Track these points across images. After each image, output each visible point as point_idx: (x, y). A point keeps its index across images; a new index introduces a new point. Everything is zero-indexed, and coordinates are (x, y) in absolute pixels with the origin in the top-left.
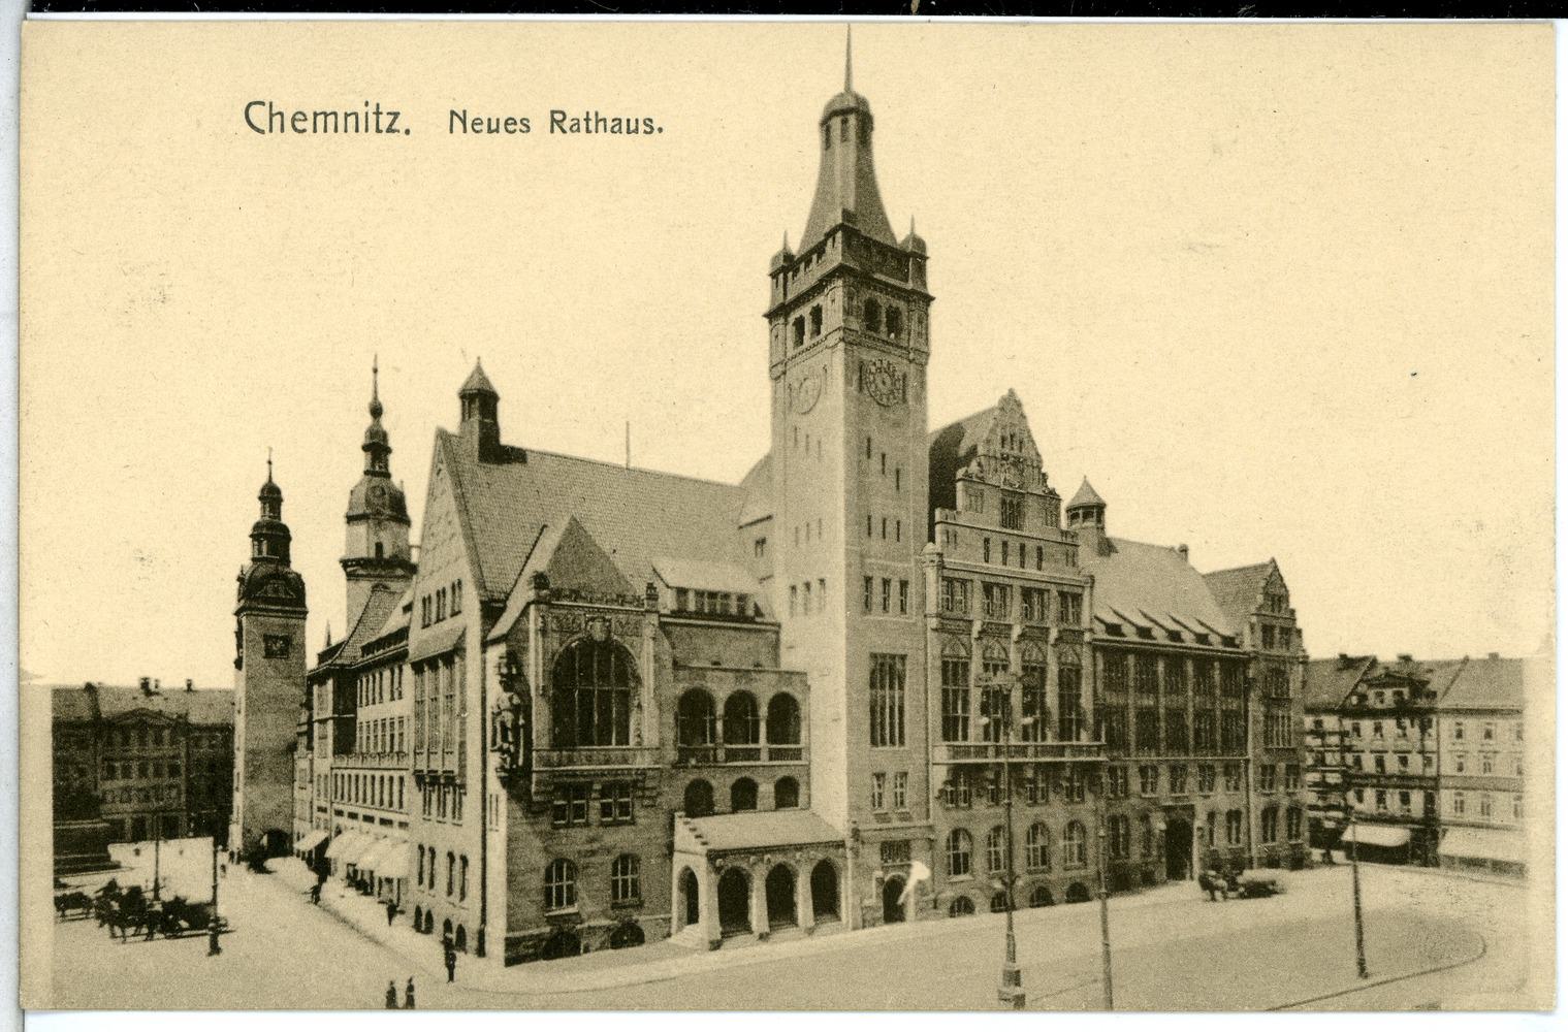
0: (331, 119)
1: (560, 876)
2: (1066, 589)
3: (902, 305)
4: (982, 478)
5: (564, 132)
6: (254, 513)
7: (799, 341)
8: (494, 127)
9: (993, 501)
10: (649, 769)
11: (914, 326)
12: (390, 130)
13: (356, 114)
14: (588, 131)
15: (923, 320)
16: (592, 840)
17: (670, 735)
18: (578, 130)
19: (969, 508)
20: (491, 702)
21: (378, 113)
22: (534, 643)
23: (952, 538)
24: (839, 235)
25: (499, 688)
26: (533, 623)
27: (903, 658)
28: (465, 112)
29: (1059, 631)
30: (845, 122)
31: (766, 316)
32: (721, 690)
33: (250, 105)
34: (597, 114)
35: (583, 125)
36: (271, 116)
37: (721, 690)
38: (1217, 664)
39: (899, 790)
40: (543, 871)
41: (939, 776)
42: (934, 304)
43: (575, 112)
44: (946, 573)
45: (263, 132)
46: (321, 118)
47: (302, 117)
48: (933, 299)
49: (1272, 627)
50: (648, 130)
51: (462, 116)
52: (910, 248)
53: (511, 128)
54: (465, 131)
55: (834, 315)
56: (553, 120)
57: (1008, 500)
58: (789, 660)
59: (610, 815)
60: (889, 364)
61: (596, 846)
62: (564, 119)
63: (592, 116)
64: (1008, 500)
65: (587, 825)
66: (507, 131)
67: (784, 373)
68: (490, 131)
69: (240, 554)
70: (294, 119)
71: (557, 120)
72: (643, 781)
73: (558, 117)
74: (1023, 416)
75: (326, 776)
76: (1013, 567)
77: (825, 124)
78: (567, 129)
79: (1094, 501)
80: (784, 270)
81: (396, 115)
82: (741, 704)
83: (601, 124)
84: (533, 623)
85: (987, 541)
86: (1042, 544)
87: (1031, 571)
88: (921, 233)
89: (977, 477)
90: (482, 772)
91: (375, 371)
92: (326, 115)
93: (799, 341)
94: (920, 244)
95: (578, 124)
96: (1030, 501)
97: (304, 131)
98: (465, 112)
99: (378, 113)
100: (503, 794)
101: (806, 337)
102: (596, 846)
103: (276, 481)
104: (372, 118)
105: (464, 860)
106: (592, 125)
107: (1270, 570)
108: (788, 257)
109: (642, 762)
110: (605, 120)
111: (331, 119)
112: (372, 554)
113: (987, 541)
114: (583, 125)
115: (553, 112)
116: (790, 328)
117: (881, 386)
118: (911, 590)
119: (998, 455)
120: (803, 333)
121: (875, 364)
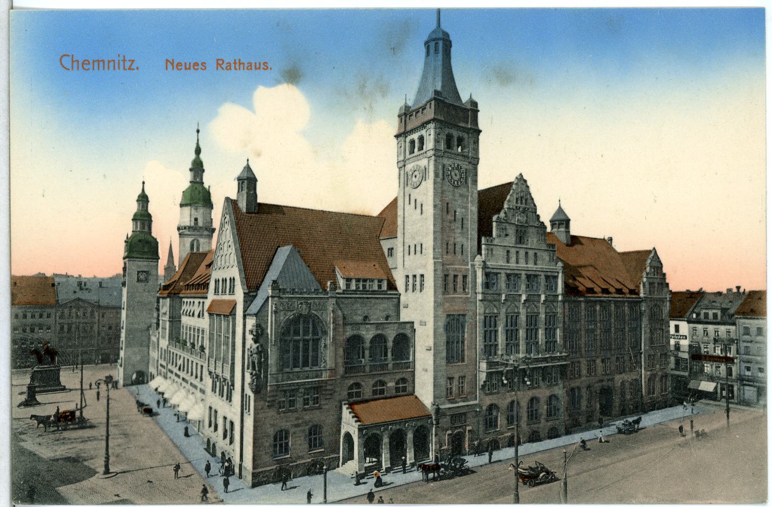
0: (101, 64)
1: (280, 441)
2: (549, 274)
3: (466, 136)
4: (506, 220)
5: (223, 69)
6: (134, 207)
7: (412, 152)
8: (188, 66)
9: (511, 231)
10: (328, 380)
11: (471, 146)
12: (130, 69)
13: (114, 61)
14: (235, 69)
15: (476, 142)
16: (297, 419)
17: (340, 361)
18: (230, 69)
19: (499, 236)
20: (248, 346)
21: (124, 60)
22: (270, 318)
23: (490, 251)
24: (433, 102)
25: (252, 342)
26: (271, 306)
27: (464, 315)
28: (173, 60)
29: (546, 297)
30: (436, 44)
31: (395, 136)
32: (368, 334)
33: (62, 56)
34: (240, 60)
35: (233, 66)
36: (73, 62)
37: (368, 334)
38: (626, 304)
39: (461, 385)
40: (272, 436)
41: (483, 377)
42: (481, 134)
43: (229, 59)
44: (487, 270)
45: (68, 69)
46: (96, 64)
47: (87, 62)
48: (481, 131)
49: (654, 283)
50: (265, 68)
51: (171, 61)
52: (469, 107)
53: (196, 67)
54: (173, 69)
55: (429, 144)
56: (218, 64)
57: (519, 229)
58: (405, 316)
59: (308, 404)
60: (458, 165)
61: (300, 421)
62: (223, 63)
63: (237, 61)
64: (519, 229)
65: (296, 411)
66: (194, 68)
67: (405, 166)
68: (186, 69)
69: (128, 228)
70: (83, 64)
71: (219, 63)
72: (326, 386)
73: (220, 62)
74: (528, 187)
75: (165, 350)
76: (522, 265)
77: (427, 43)
78: (225, 68)
79: (563, 217)
80: (405, 114)
81: (133, 61)
82: (379, 339)
83: (242, 66)
84: (271, 306)
85: (508, 252)
86: (536, 251)
87: (531, 265)
88: (475, 98)
89: (503, 219)
90: (243, 379)
91: (198, 131)
92: (98, 61)
93: (412, 152)
94: (475, 104)
95: (230, 65)
96: (531, 230)
97: (88, 69)
98: (173, 60)
99: (124, 60)
100: (252, 396)
101: (416, 150)
102: (300, 421)
103: (147, 192)
104: (122, 63)
105: (232, 423)
106: (237, 67)
107: (652, 255)
108: (407, 107)
109: (325, 376)
110: (78, 61)
111: (101, 64)
112: (193, 224)
113: (508, 252)
114: (233, 66)
115: (217, 60)
116: (408, 144)
117: (454, 176)
118: (469, 279)
119: (514, 208)
120: (414, 148)
121: (451, 166)
